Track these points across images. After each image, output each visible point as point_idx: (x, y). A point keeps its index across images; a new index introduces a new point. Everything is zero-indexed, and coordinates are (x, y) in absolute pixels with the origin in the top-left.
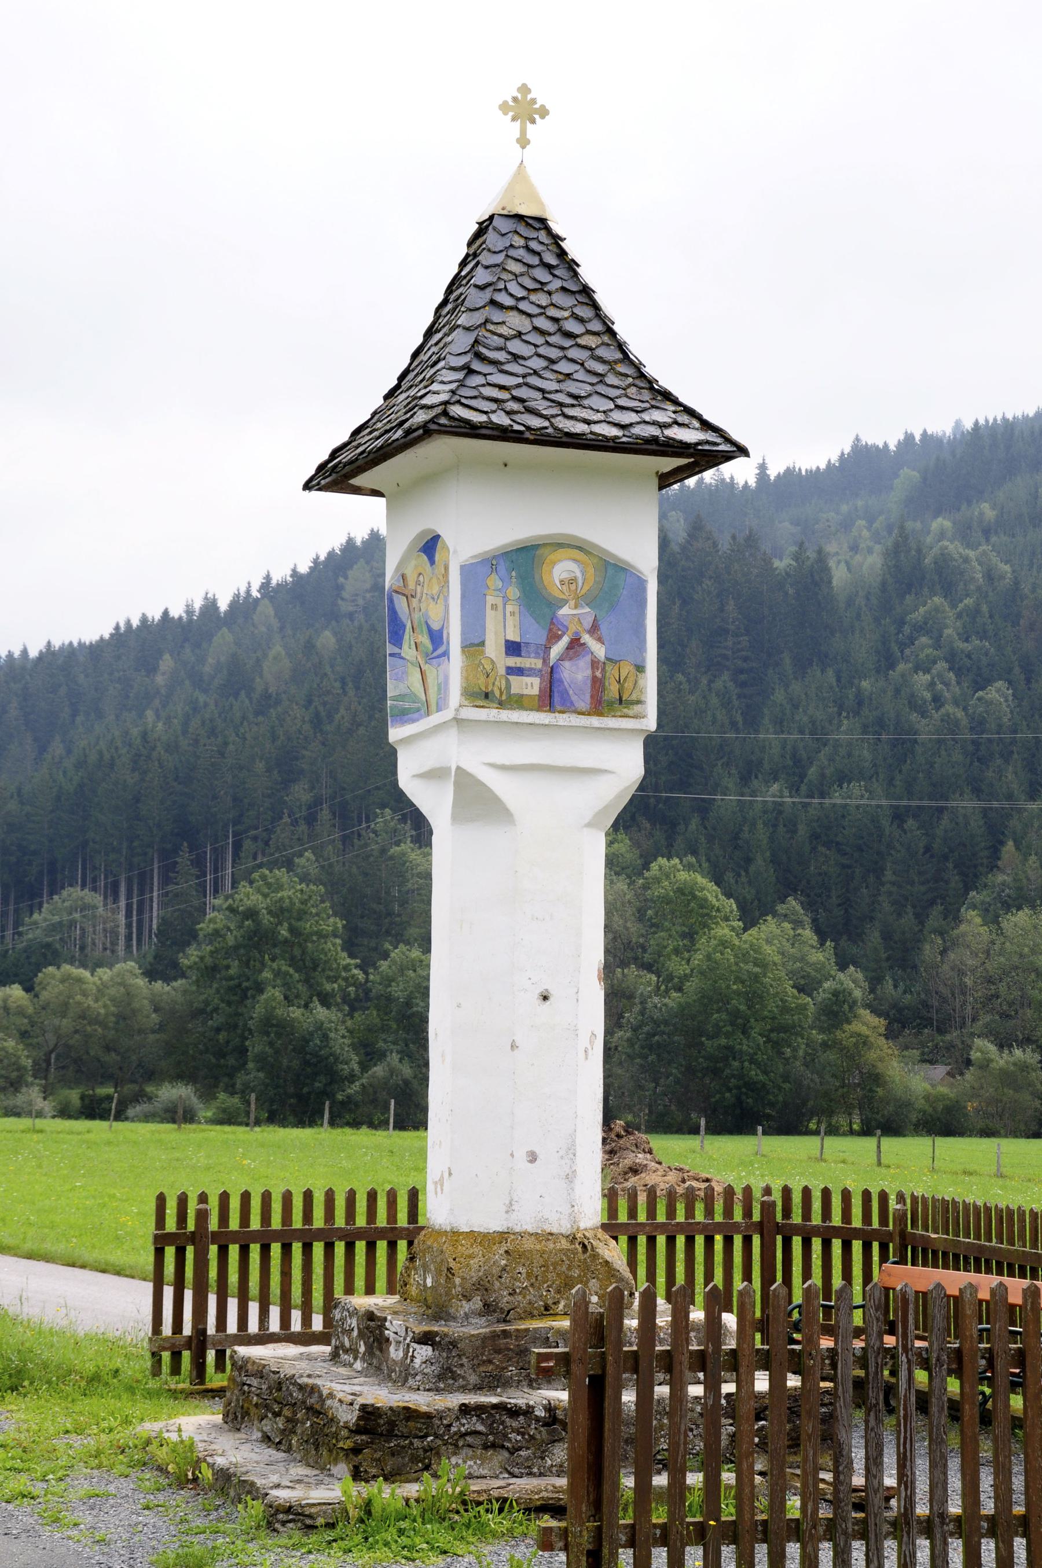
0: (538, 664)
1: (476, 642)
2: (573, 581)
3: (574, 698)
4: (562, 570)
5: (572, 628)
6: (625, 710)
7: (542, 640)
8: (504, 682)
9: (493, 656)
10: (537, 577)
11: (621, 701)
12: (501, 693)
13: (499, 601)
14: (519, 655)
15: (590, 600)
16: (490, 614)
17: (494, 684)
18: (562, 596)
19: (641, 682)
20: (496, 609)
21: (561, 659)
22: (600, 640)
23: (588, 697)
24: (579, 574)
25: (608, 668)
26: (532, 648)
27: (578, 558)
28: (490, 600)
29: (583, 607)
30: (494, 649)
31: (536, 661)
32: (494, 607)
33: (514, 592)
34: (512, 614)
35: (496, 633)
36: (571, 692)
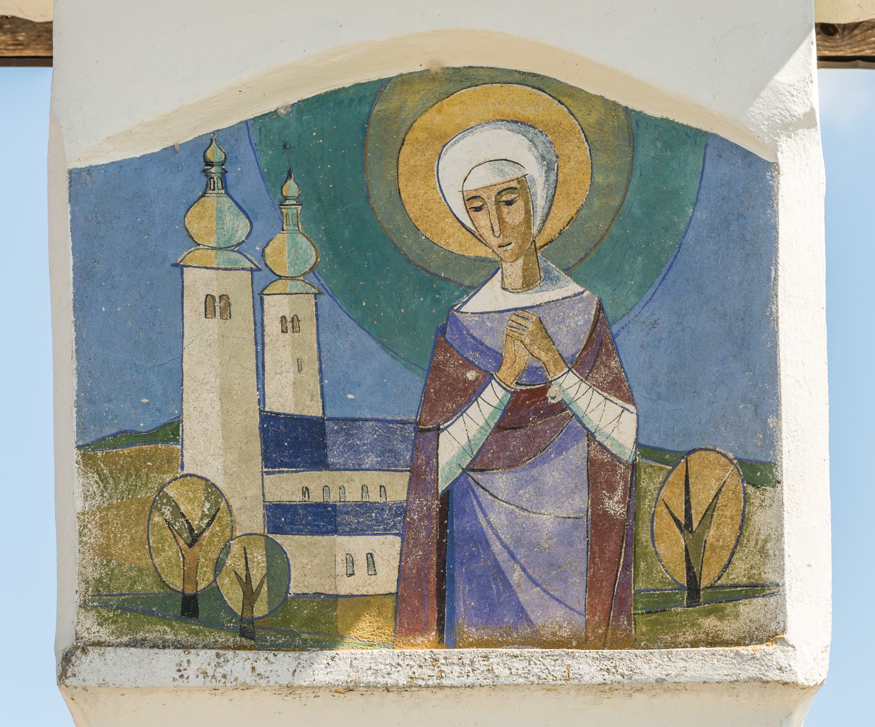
0: (396, 487)
1: (142, 427)
2: (514, 192)
3: (528, 596)
4: (468, 161)
5: (517, 358)
6: (710, 623)
7: (407, 408)
8: (259, 557)
9: (214, 472)
10: (379, 193)
11: (693, 589)
12: (250, 597)
13: (238, 286)
14: (320, 463)
15: (581, 252)
16: (200, 334)
17: (218, 566)
18: (481, 251)
19: (760, 519)
20: (296, 329)
21: (480, 462)
22: (618, 388)
23: (576, 590)
24: (535, 170)
25: (648, 483)
26: (368, 436)
27: (529, 113)
28: (199, 283)
29: (550, 279)
30: (214, 445)
31: (384, 478)
32: (217, 306)
33: (292, 249)
34: (290, 324)
35: (225, 393)
36: (516, 576)
